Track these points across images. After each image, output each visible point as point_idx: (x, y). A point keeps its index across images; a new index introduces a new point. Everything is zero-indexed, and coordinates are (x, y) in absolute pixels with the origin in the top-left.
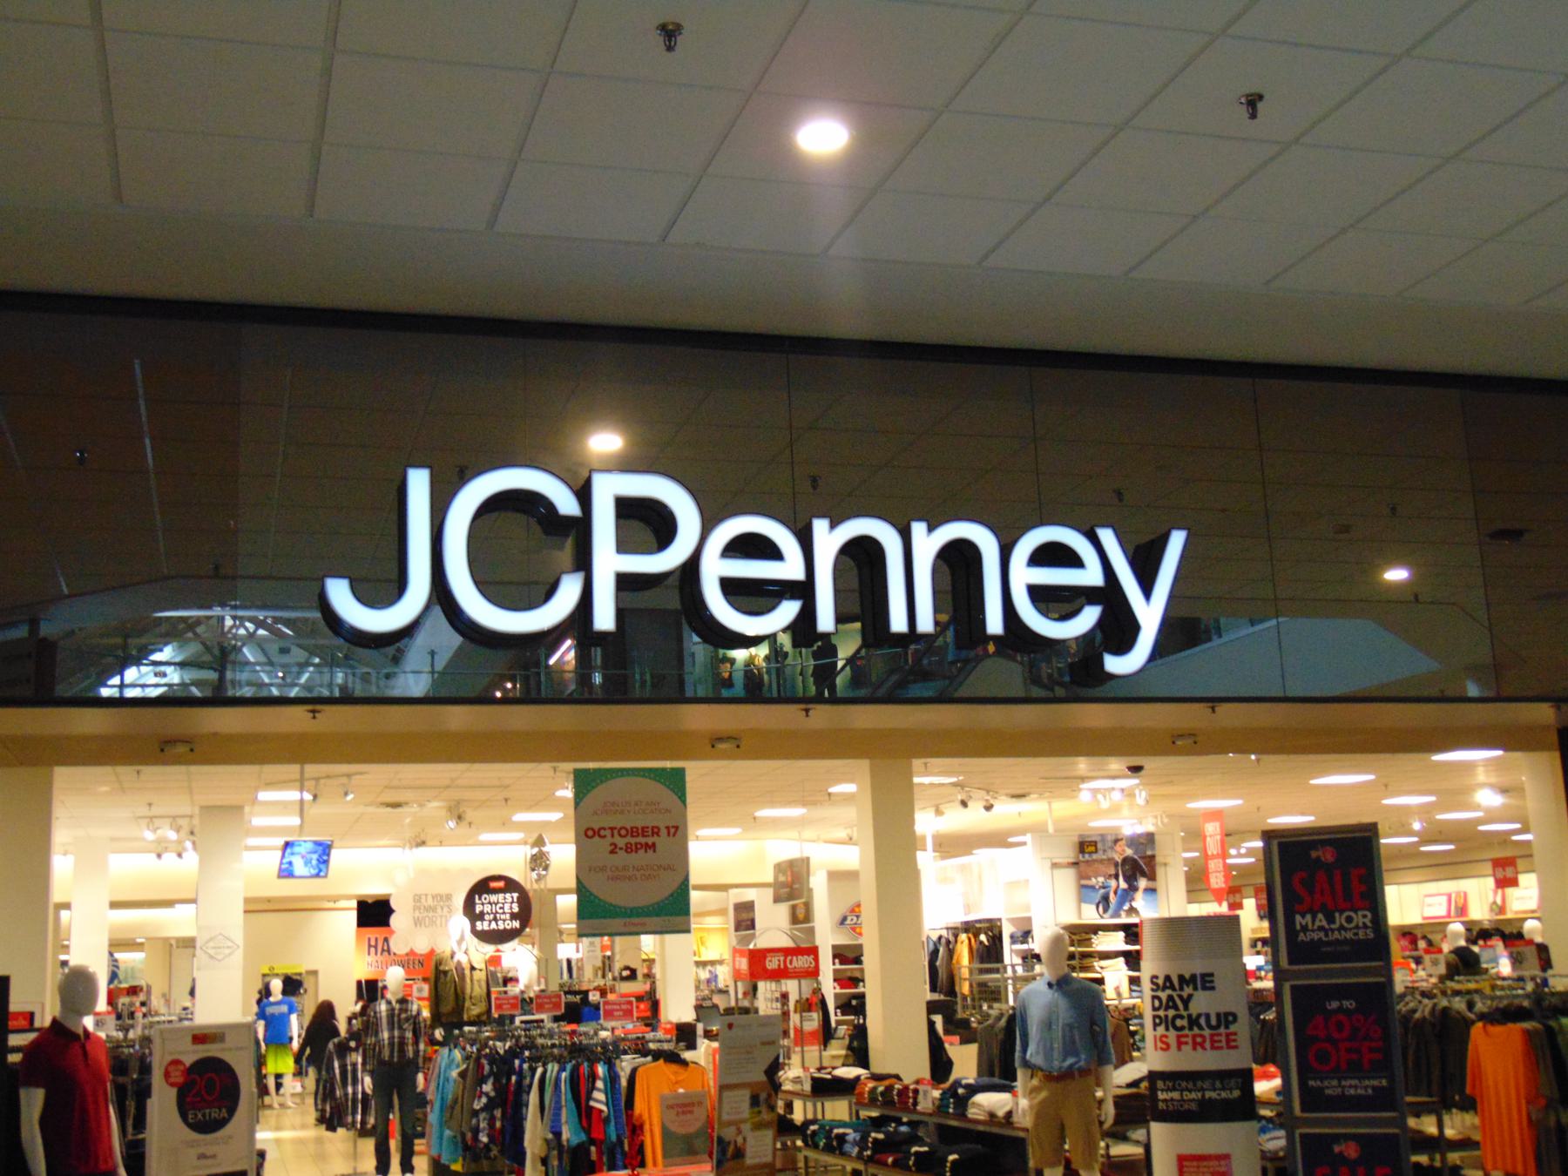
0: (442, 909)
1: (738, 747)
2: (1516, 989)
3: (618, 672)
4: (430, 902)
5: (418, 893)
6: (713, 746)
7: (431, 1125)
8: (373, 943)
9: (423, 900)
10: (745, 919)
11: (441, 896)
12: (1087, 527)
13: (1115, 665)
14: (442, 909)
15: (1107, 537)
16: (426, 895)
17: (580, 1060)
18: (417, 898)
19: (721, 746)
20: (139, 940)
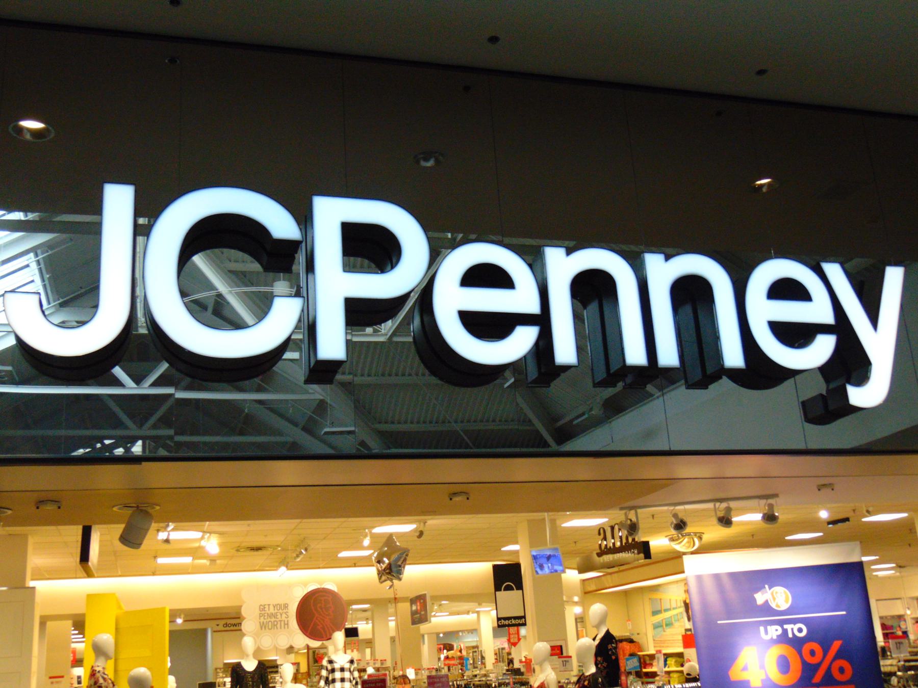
0: (281, 615)
1: (468, 499)
2: (638, 560)
3: (263, 384)
4: (272, 610)
5: (263, 604)
6: (451, 499)
7: (613, 558)
8: (286, 626)
9: (267, 609)
10: (461, 651)
11: (280, 605)
12: (814, 263)
13: (858, 396)
14: (281, 615)
15: (834, 271)
16: (269, 605)
17: (633, 543)
18: (262, 608)
19: (457, 499)
20: (830, 526)
